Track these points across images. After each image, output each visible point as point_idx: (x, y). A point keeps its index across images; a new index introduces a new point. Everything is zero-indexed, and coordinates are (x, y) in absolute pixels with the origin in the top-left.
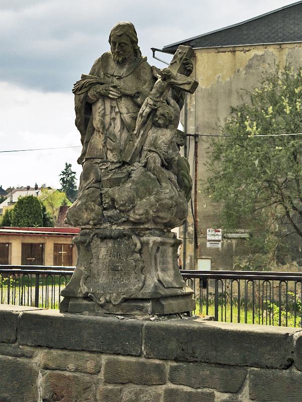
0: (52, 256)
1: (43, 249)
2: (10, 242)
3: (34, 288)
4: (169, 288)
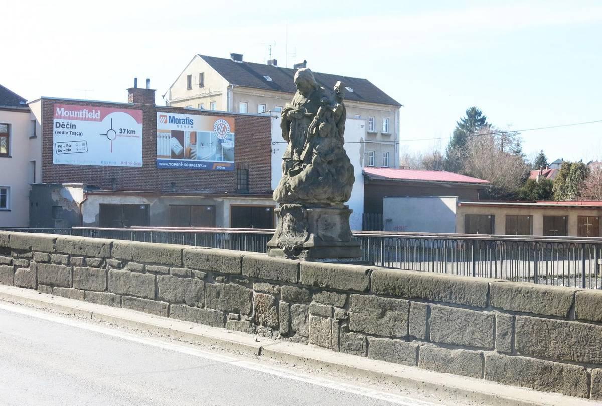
0: (576, 228)
1: (566, 222)
2: (531, 214)
3: (471, 263)
4: (241, 267)
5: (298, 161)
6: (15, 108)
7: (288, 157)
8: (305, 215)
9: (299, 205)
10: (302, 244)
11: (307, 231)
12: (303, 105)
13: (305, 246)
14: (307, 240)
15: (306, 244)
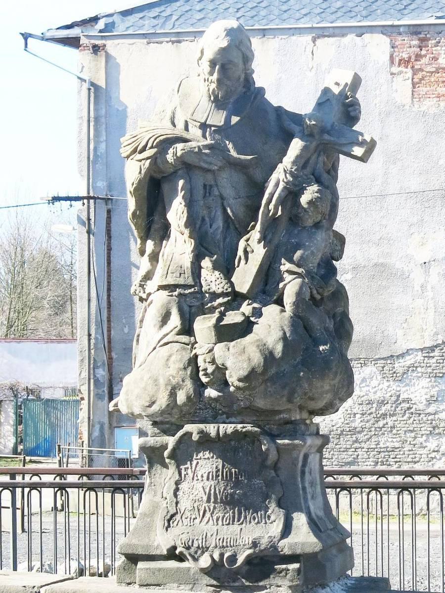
5: (223, 295)
6: (91, 177)
7: (181, 281)
8: (273, 456)
9: (249, 427)
10: (274, 547)
11: (279, 505)
12: (219, 130)
13: (286, 551)
14: (287, 530)
15: (291, 546)
